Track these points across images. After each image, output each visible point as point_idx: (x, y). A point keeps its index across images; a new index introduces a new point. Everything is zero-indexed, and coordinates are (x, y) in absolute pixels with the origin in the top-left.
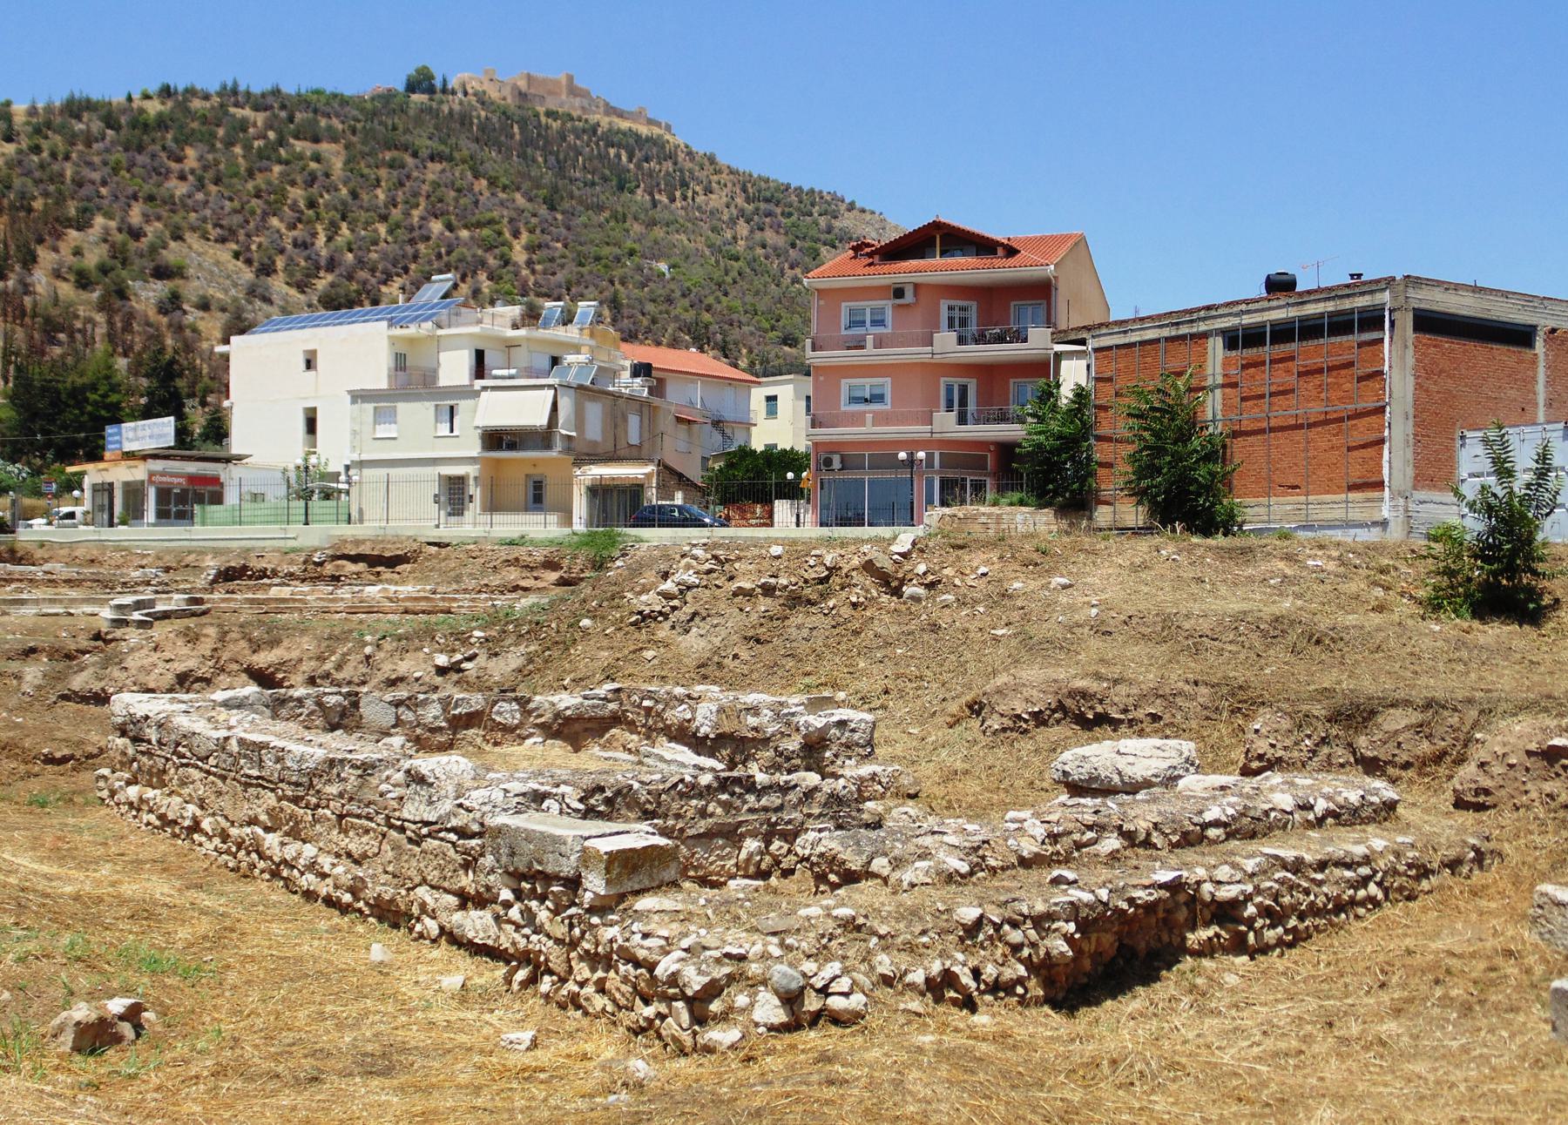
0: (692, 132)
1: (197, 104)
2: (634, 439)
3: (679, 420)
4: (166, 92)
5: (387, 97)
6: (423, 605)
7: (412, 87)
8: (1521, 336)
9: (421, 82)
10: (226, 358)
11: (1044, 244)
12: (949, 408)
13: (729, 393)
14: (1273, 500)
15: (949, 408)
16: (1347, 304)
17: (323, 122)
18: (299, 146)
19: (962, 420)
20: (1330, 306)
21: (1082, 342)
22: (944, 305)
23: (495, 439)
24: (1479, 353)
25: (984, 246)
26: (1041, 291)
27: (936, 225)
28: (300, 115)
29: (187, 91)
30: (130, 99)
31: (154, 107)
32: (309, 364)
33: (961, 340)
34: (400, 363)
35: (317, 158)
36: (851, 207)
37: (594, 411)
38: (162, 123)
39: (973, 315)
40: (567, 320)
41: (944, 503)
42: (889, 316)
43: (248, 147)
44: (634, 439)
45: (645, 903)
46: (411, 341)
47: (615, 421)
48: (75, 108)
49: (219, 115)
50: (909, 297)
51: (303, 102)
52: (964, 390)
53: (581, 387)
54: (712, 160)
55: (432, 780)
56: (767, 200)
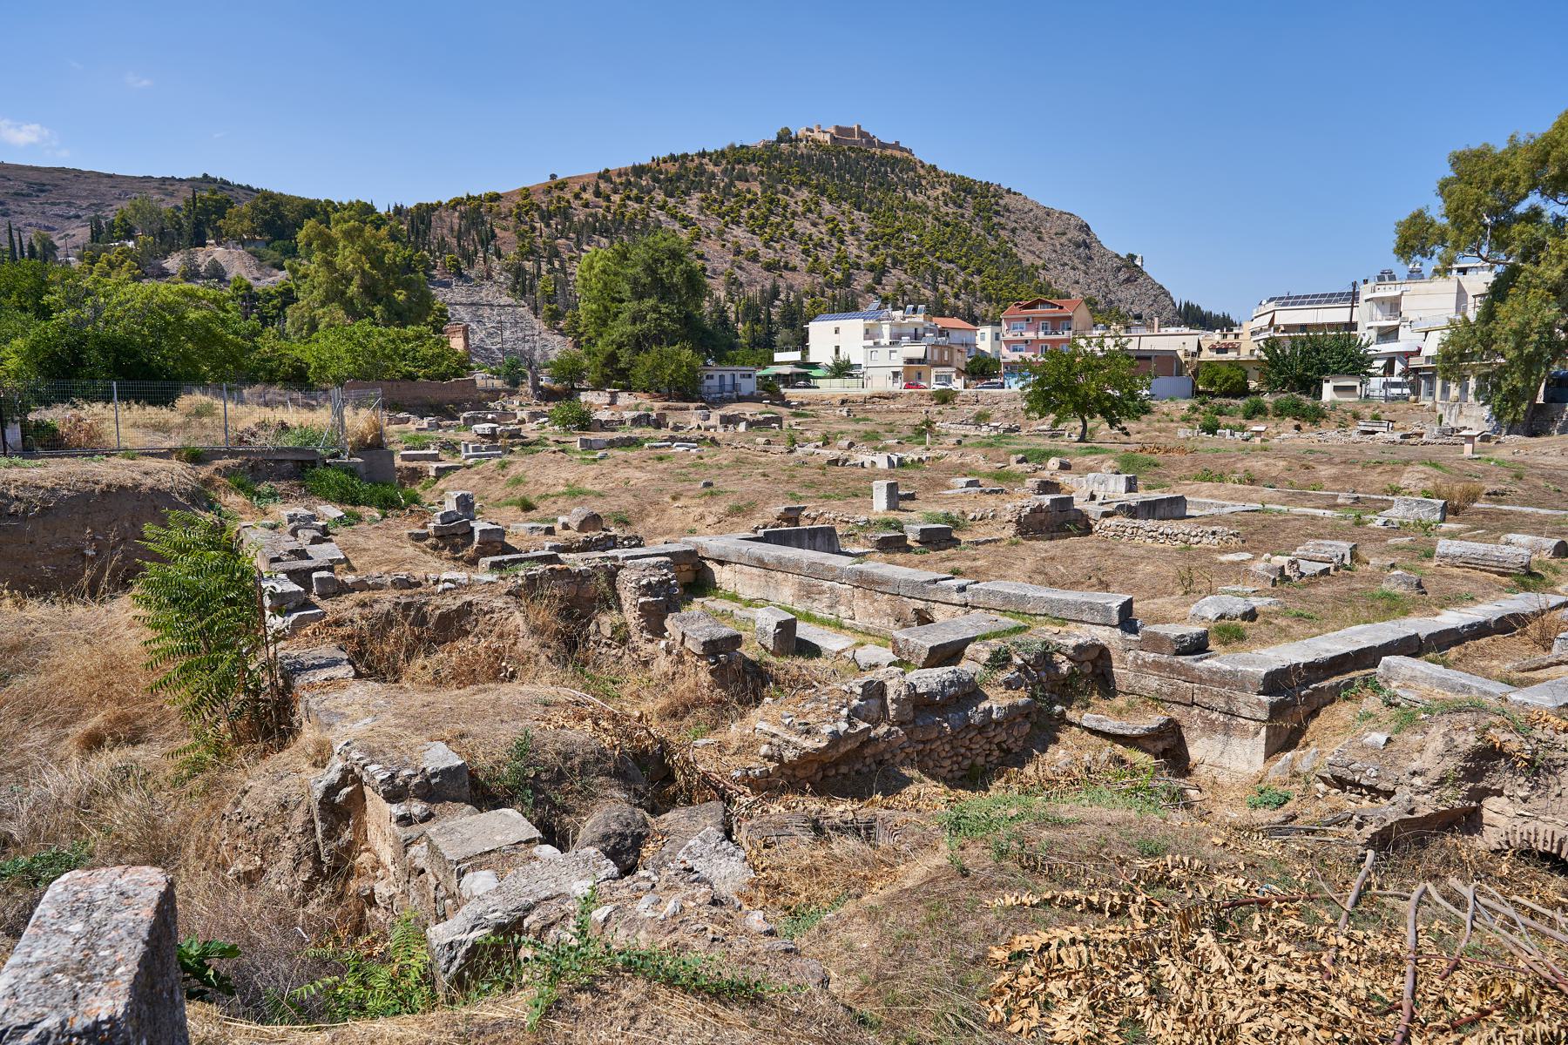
0: (924, 154)
4: (673, 158)
7: (780, 139)
8: (1149, 358)
9: (784, 136)
23: (910, 361)
31: (672, 168)
37: (936, 351)
38: (679, 177)
43: (718, 188)
47: (941, 354)
48: (639, 171)
54: (934, 168)
56: (964, 188)
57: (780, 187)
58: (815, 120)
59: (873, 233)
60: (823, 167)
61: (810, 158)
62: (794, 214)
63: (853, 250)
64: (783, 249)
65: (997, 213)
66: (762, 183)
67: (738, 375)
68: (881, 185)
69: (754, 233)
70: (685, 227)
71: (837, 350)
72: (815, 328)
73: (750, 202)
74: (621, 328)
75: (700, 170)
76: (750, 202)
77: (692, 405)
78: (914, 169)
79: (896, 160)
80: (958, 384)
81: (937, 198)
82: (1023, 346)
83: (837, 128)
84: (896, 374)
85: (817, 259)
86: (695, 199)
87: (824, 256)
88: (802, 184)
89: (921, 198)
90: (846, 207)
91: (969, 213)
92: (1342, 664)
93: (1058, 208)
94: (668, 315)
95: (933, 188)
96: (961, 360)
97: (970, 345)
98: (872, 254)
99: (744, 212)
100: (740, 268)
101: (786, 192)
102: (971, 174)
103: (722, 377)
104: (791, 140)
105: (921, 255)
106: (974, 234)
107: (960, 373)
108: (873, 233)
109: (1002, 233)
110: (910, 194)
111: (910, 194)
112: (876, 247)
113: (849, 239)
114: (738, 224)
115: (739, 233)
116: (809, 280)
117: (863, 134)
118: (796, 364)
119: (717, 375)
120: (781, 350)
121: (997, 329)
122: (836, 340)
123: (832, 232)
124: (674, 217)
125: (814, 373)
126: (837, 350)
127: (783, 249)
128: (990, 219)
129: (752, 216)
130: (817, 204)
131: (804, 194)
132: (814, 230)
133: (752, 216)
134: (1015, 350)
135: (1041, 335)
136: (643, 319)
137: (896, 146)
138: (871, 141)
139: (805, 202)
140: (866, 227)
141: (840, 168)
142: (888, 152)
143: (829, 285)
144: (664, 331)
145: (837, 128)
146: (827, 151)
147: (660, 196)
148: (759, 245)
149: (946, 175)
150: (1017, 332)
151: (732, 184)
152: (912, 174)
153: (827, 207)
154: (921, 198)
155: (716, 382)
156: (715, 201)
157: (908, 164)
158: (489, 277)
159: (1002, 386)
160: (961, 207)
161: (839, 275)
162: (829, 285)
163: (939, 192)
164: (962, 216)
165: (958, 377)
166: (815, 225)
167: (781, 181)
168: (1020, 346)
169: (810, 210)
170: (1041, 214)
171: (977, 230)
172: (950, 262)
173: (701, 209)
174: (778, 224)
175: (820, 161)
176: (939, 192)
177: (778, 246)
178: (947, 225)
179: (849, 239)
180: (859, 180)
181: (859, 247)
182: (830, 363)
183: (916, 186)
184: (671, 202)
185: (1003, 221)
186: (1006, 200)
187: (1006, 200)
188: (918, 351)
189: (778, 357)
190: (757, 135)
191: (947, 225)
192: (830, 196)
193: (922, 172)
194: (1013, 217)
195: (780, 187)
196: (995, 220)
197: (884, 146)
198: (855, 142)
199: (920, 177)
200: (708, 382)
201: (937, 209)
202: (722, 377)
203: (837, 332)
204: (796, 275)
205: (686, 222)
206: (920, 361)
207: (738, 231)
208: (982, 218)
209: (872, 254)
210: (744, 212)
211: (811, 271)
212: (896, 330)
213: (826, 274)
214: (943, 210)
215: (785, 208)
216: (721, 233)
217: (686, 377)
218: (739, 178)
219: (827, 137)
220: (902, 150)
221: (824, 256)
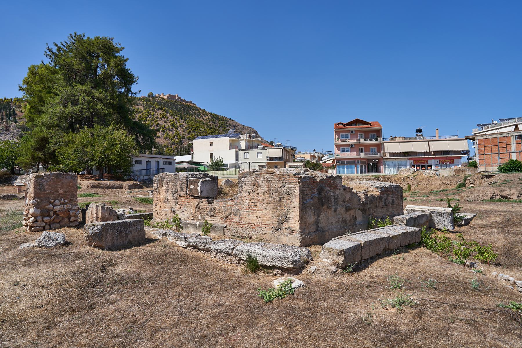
0: (200, 105)
7: (149, 96)
23: (271, 158)
27: (357, 120)
36: (230, 119)
42: (349, 136)
46: (233, 140)
50: (354, 133)
57: (151, 109)
63: (181, 132)
65: (227, 126)
66: (143, 107)
67: (161, 162)
71: (211, 155)
74: (55, 108)
77: (125, 184)
78: (198, 110)
79: (191, 107)
81: (206, 120)
85: (168, 134)
87: (170, 133)
88: (159, 109)
91: (218, 125)
93: (247, 125)
94: (100, 100)
95: (205, 116)
98: (189, 134)
101: (153, 110)
102: (217, 113)
103: (148, 163)
104: (153, 97)
110: (197, 118)
111: (197, 118)
113: (180, 128)
116: (165, 141)
118: (189, 162)
119: (144, 161)
122: (210, 150)
123: (173, 125)
126: (211, 155)
128: (225, 128)
131: (160, 112)
134: (343, 151)
135: (362, 141)
136: (75, 103)
138: (182, 100)
139: (161, 114)
140: (184, 124)
143: (174, 143)
144: (96, 113)
146: (167, 101)
149: (209, 113)
150: (344, 139)
153: (170, 117)
155: (144, 166)
157: (196, 109)
158: (7, 129)
161: (177, 140)
162: (174, 143)
163: (207, 118)
164: (216, 126)
166: (166, 122)
167: (151, 107)
169: (163, 117)
170: (241, 127)
174: (151, 121)
176: (207, 118)
178: (212, 128)
179: (180, 128)
181: (184, 131)
183: (199, 115)
186: (229, 122)
187: (229, 122)
195: (151, 109)
197: (187, 102)
200: (137, 166)
201: (207, 123)
202: (148, 163)
203: (211, 144)
204: (159, 139)
206: (280, 158)
208: (222, 127)
209: (189, 134)
211: (166, 138)
213: (172, 139)
215: (154, 115)
217: (119, 155)
219: (166, 97)
220: (193, 104)
221: (170, 133)
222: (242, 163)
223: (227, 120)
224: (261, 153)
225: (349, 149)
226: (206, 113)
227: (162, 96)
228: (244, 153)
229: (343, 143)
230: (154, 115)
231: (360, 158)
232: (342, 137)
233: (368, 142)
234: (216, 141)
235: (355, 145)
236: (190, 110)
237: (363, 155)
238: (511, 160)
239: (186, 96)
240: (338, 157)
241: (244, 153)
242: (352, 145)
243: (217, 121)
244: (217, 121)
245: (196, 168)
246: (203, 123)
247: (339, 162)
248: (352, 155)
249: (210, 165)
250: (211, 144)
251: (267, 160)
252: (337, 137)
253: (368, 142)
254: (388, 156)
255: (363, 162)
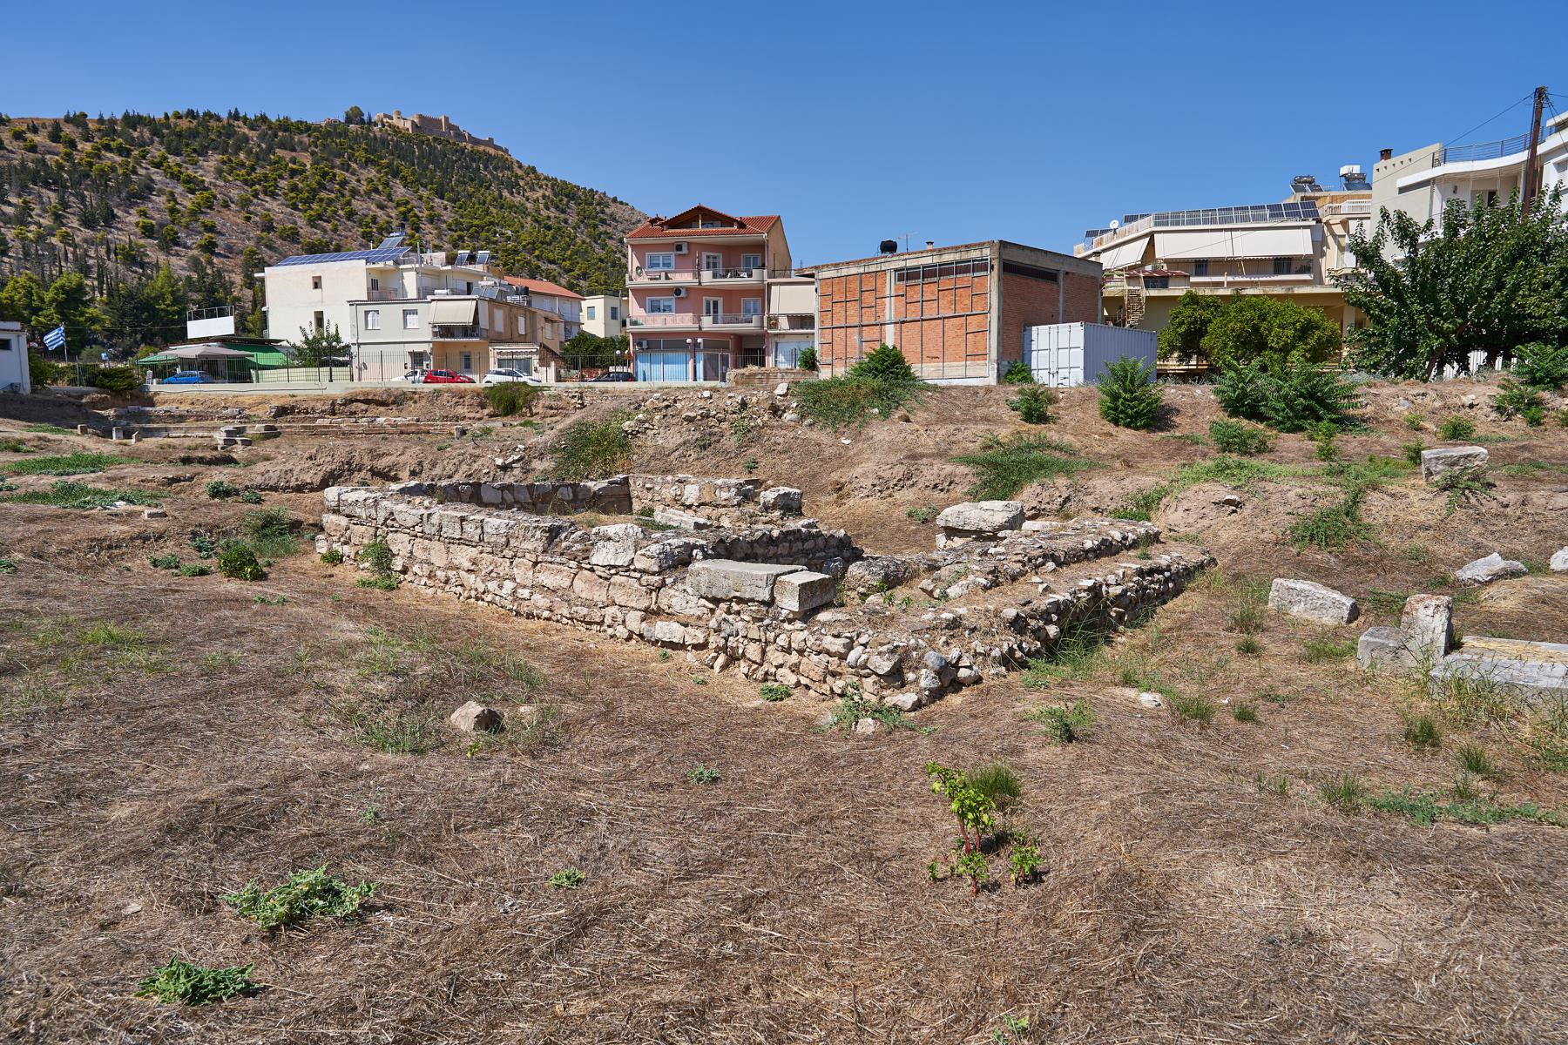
0: (522, 154)
1: (213, 123)
2: (522, 332)
3: (547, 319)
4: (191, 114)
5: (333, 125)
6: (413, 429)
7: (349, 120)
8: (1051, 276)
9: (355, 116)
10: (262, 280)
11: (760, 221)
12: (708, 312)
13: (567, 305)
14: (1034, 366)
15: (708, 312)
16: (965, 256)
17: (296, 138)
18: (280, 152)
19: (715, 321)
20: (957, 257)
21: (812, 276)
22: (704, 255)
23: (446, 330)
24: (1032, 283)
25: (728, 221)
26: (760, 247)
27: (699, 209)
28: (283, 132)
29: (205, 114)
30: (167, 117)
31: (184, 124)
32: (317, 285)
33: (715, 276)
34: (374, 285)
35: (294, 161)
36: (615, 200)
37: (499, 315)
38: (194, 134)
39: (720, 261)
40: (472, 259)
41: (736, 367)
43: (249, 152)
44: (522, 332)
45: (823, 616)
46: (381, 271)
47: (511, 322)
48: (132, 121)
49: (229, 131)
50: (685, 251)
51: (285, 125)
52: (715, 304)
53: (491, 300)
54: (533, 170)
55: (1206, 557)
56: (565, 193)
57: (338, 162)
58: (397, 105)
59: (458, 223)
60: (405, 155)
61: (384, 142)
62: (354, 192)
64: (335, 230)
65: (603, 222)
66: (313, 153)
68: (472, 180)
69: (295, 207)
70: (192, 192)
71: (319, 318)
72: (274, 277)
73: (293, 173)
75: (229, 131)
76: (293, 173)
78: (510, 168)
79: (488, 159)
80: (544, 376)
82: (671, 301)
83: (421, 117)
84: (418, 358)
86: (213, 161)
88: (368, 162)
89: (518, 199)
90: (425, 193)
91: (573, 219)
92: (783, 548)
95: (532, 189)
96: (551, 336)
97: (572, 324)
99: (283, 183)
100: (270, 247)
104: (362, 122)
105: (516, 252)
106: (578, 241)
107: (547, 355)
108: (458, 223)
109: (609, 242)
110: (506, 193)
111: (506, 193)
112: (461, 238)
113: (427, 227)
114: (273, 195)
115: (276, 208)
117: (450, 127)
118: (224, 341)
120: (198, 316)
121: (615, 302)
122: (313, 301)
124: (175, 177)
125: (261, 358)
126: (319, 318)
127: (335, 230)
128: (595, 227)
129: (294, 188)
130: (386, 184)
131: (372, 172)
132: (380, 213)
133: (294, 188)
134: (655, 309)
135: (707, 276)
137: (490, 143)
138: (460, 135)
139: (370, 181)
140: (448, 216)
141: (422, 156)
142: (481, 148)
145: (421, 117)
146: (408, 139)
147: (156, 151)
148: (301, 222)
149: (546, 178)
151: (270, 150)
152: (507, 173)
153: (400, 191)
154: (518, 199)
156: (243, 165)
157: (504, 163)
159: (630, 377)
160: (563, 212)
163: (539, 194)
164: (566, 221)
165: (544, 362)
166: (381, 207)
167: (340, 155)
168: (665, 301)
169: (376, 191)
171: (582, 237)
172: (552, 262)
173: (219, 172)
174: (330, 202)
175: (397, 145)
176: (539, 194)
177: (329, 226)
178: (549, 228)
179: (427, 227)
180: (445, 171)
182: (298, 340)
183: (512, 186)
184: (172, 159)
185: (610, 230)
188: (460, 311)
189: (195, 328)
190: (323, 110)
191: (549, 228)
192: (404, 178)
193: (520, 172)
194: (620, 227)
195: (338, 162)
196: (602, 229)
197: (476, 142)
198: (442, 134)
199: (516, 176)
201: (538, 211)
203: (317, 284)
205: (193, 185)
206: (466, 331)
207: (271, 204)
208: (587, 226)
210: (283, 183)
212: (427, 282)
214: (544, 213)
215: (344, 183)
216: (245, 203)
218: (283, 146)
219: (408, 125)
220: (497, 148)
222: (359, 345)
223: (603, 202)
224: (415, 312)
225: (673, 303)
226: (538, 178)
227: (395, 121)
228: (367, 313)
229: (655, 284)
230: (344, 183)
231: (700, 333)
232: (652, 266)
233: (729, 281)
234: (330, 269)
235: (687, 289)
236: (486, 168)
237: (707, 323)
238: (884, 348)
239: (477, 120)
240: (636, 329)
241: (367, 313)
242: (677, 291)
243: (572, 204)
244: (572, 204)
245: (243, 357)
246: (525, 213)
247: (640, 344)
248: (682, 321)
249: (298, 349)
250: (317, 284)
251: (435, 334)
252: (636, 263)
253: (729, 281)
254: (784, 324)
255: (715, 343)
